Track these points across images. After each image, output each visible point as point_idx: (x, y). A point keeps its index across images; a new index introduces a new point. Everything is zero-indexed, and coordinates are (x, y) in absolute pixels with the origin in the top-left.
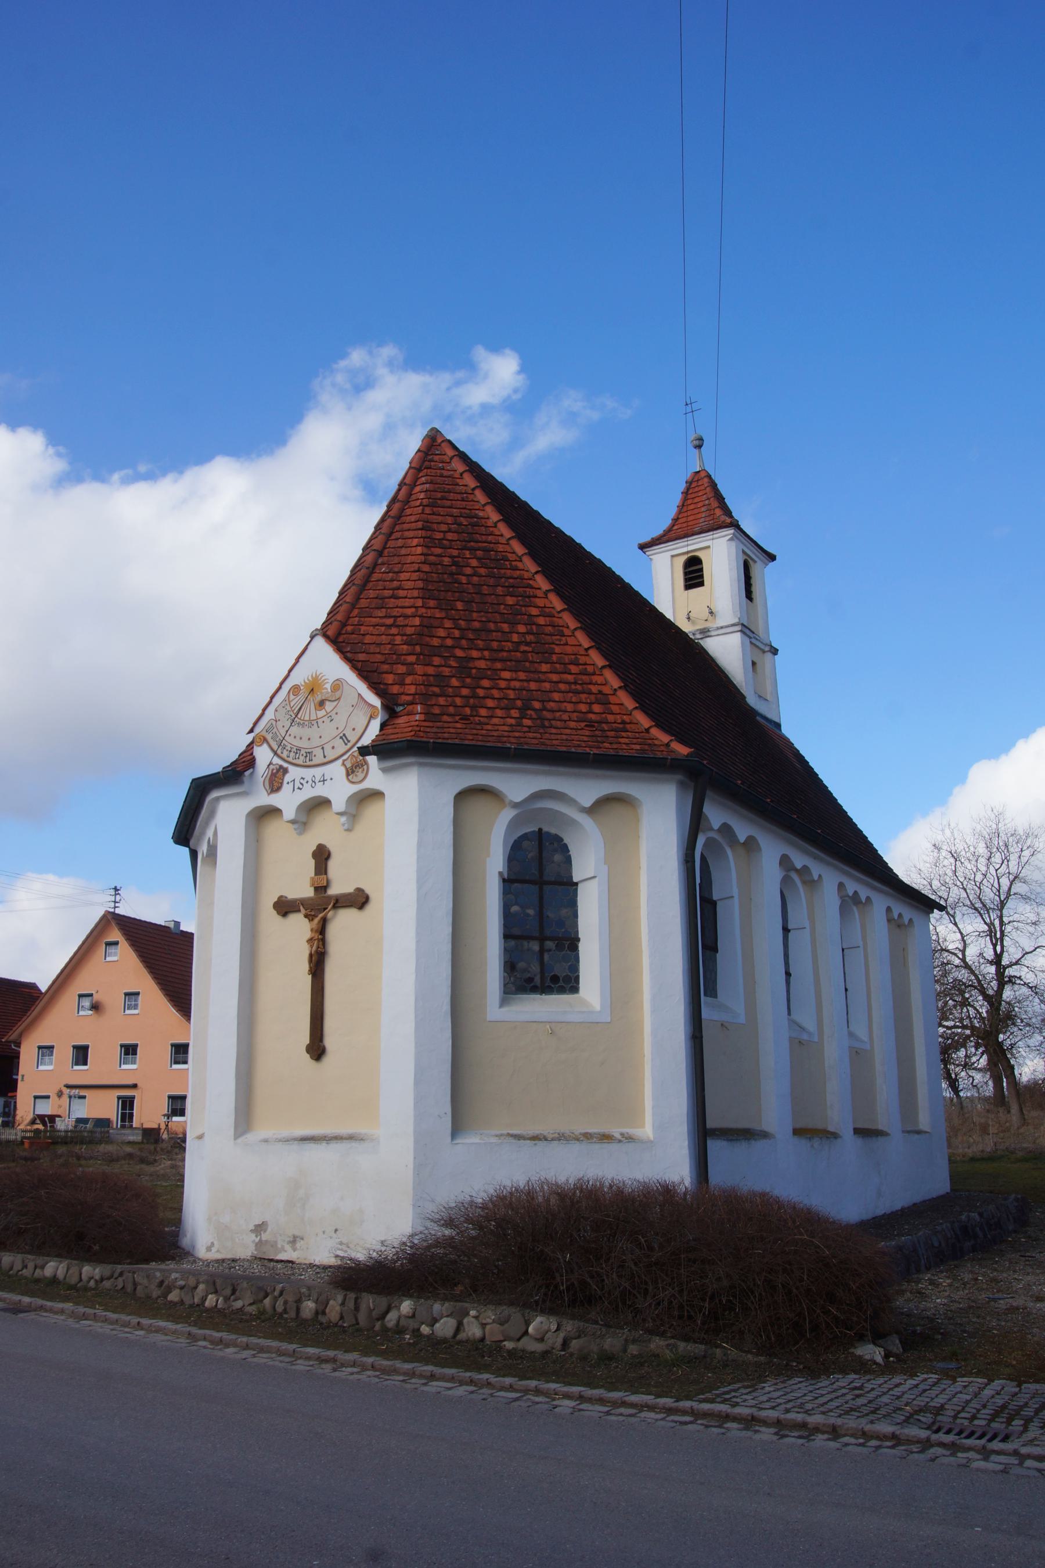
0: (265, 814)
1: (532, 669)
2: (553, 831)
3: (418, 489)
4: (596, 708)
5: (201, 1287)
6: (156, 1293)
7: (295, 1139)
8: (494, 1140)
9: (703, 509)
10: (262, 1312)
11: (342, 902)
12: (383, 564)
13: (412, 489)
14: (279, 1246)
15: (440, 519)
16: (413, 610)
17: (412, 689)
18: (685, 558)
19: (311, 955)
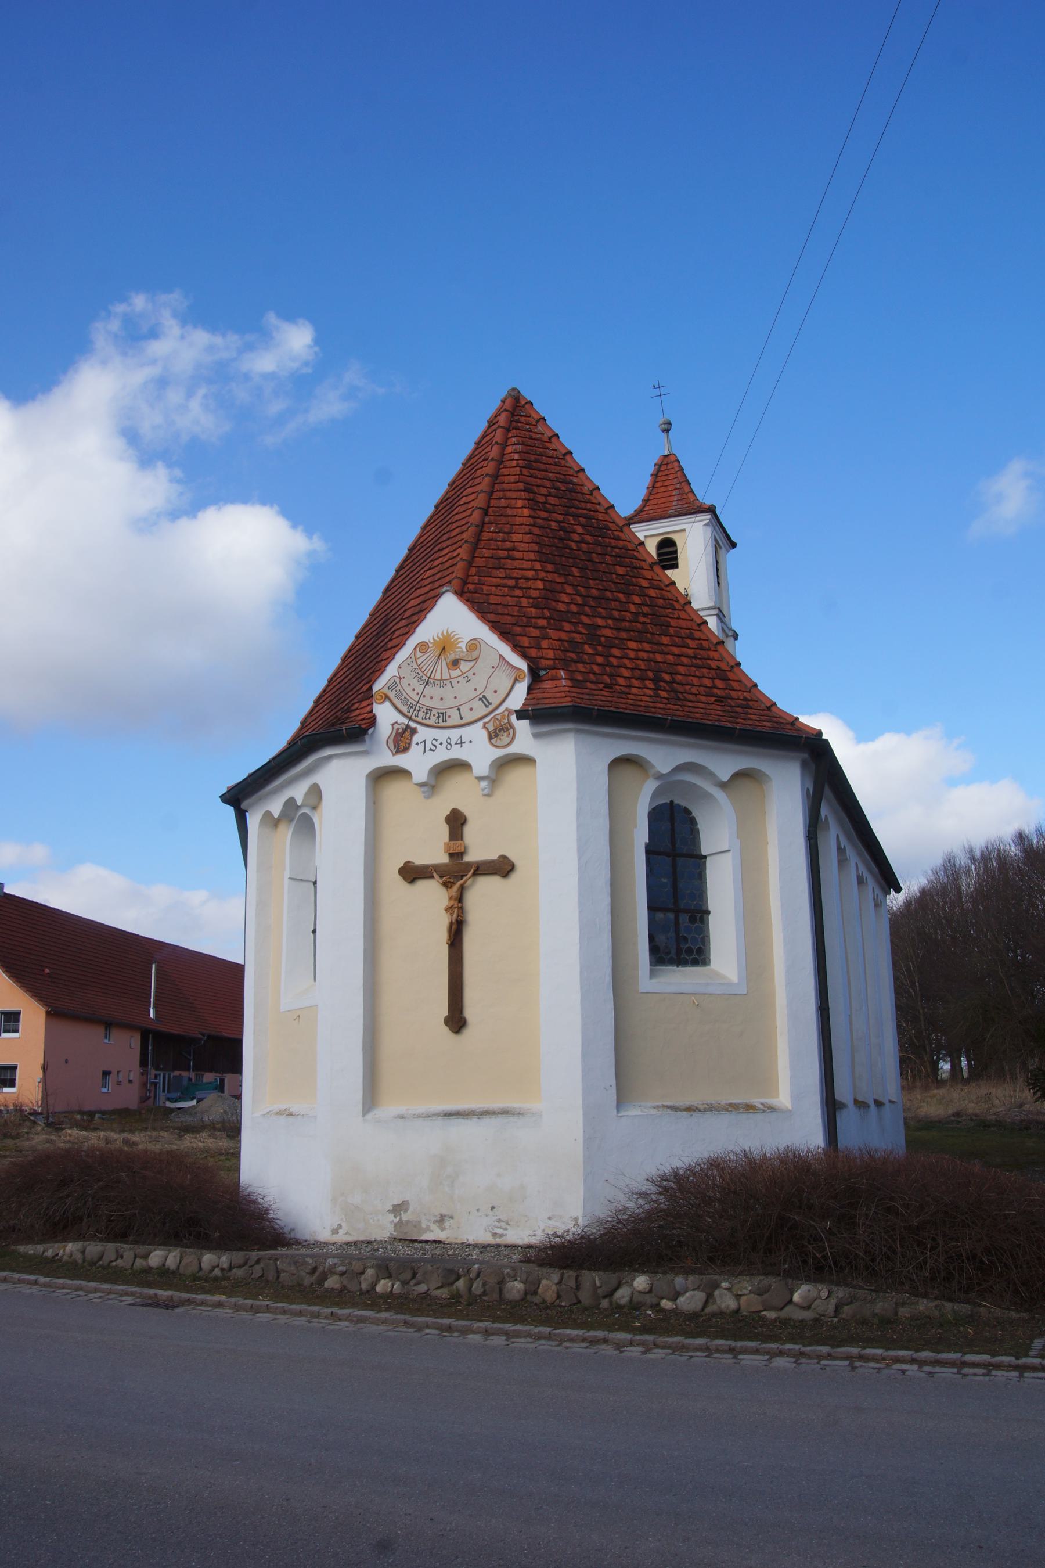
0: (381, 776)
1: (655, 641)
2: (683, 804)
3: (509, 449)
4: (719, 683)
5: (370, 1272)
6: (308, 1280)
7: (438, 1115)
8: (654, 1112)
9: (674, 493)
10: (456, 1296)
11: (482, 869)
12: (490, 523)
13: (503, 449)
14: (424, 1226)
15: (539, 482)
16: (533, 572)
17: (551, 654)
18: (658, 539)
19: (451, 924)
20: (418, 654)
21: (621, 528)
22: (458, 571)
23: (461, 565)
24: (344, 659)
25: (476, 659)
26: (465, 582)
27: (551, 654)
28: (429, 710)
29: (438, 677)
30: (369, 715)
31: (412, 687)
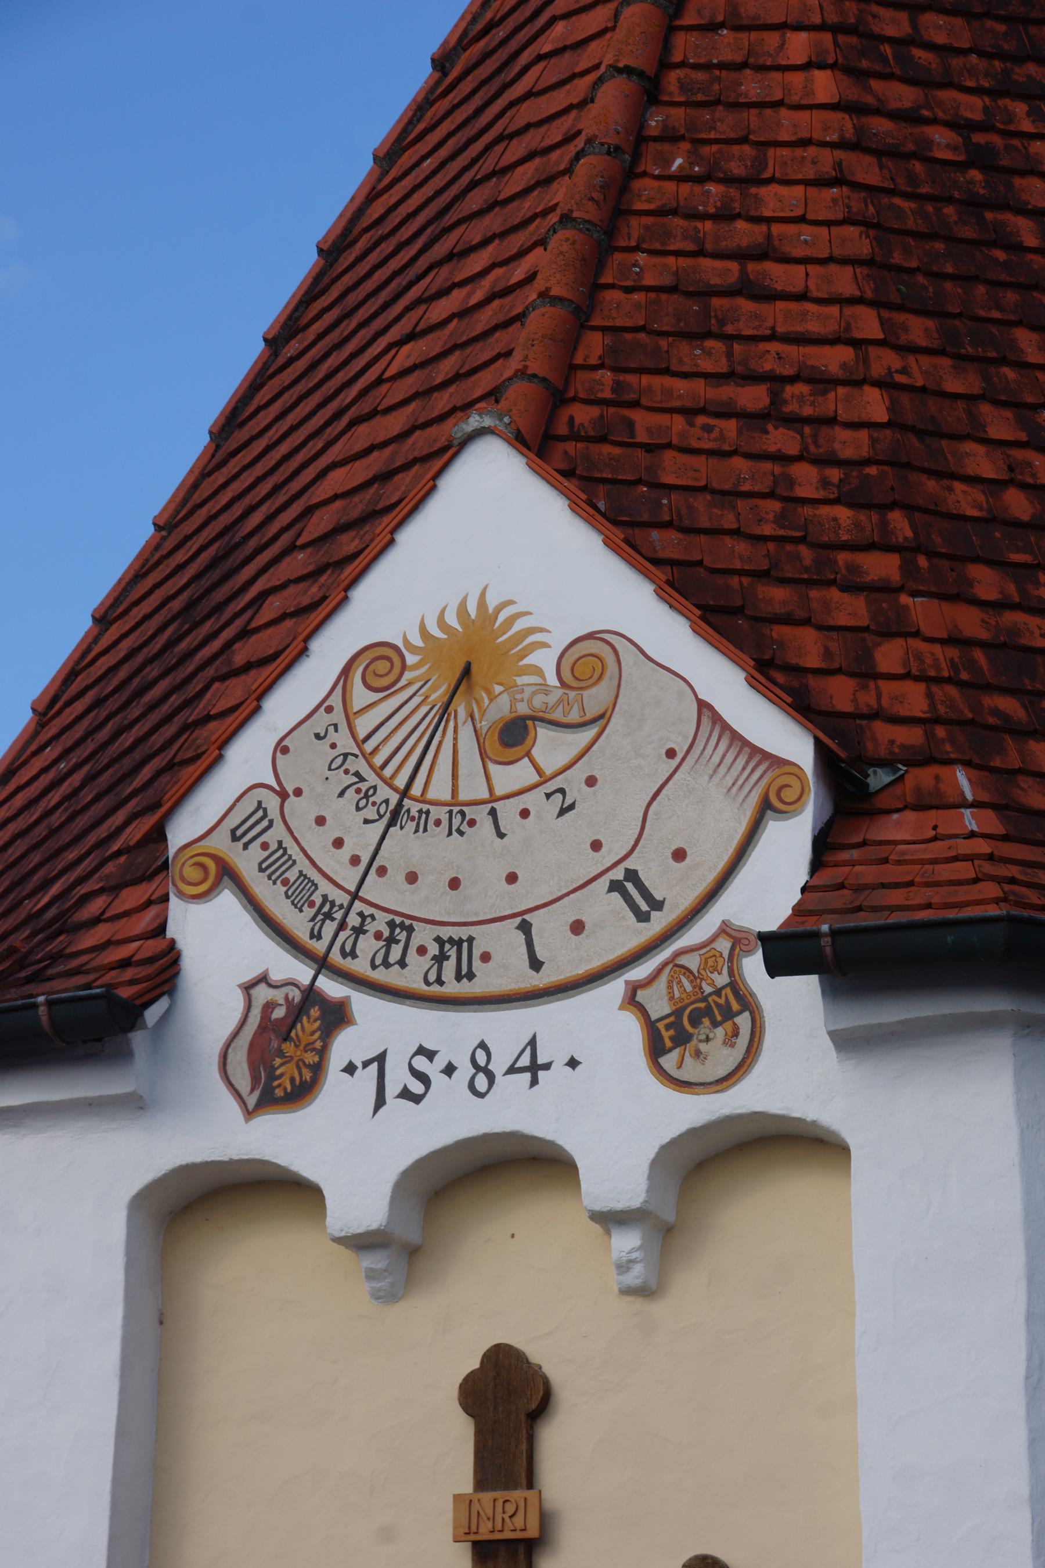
0: (192, 1207)
17: (914, 699)
20: (361, 696)
22: (532, 345)
23: (542, 321)
24: (47, 710)
25: (603, 718)
26: (557, 396)
27: (914, 699)
28: (402, 926)
29: (440, 790)
30: (151, 947)
31: (332, 833)
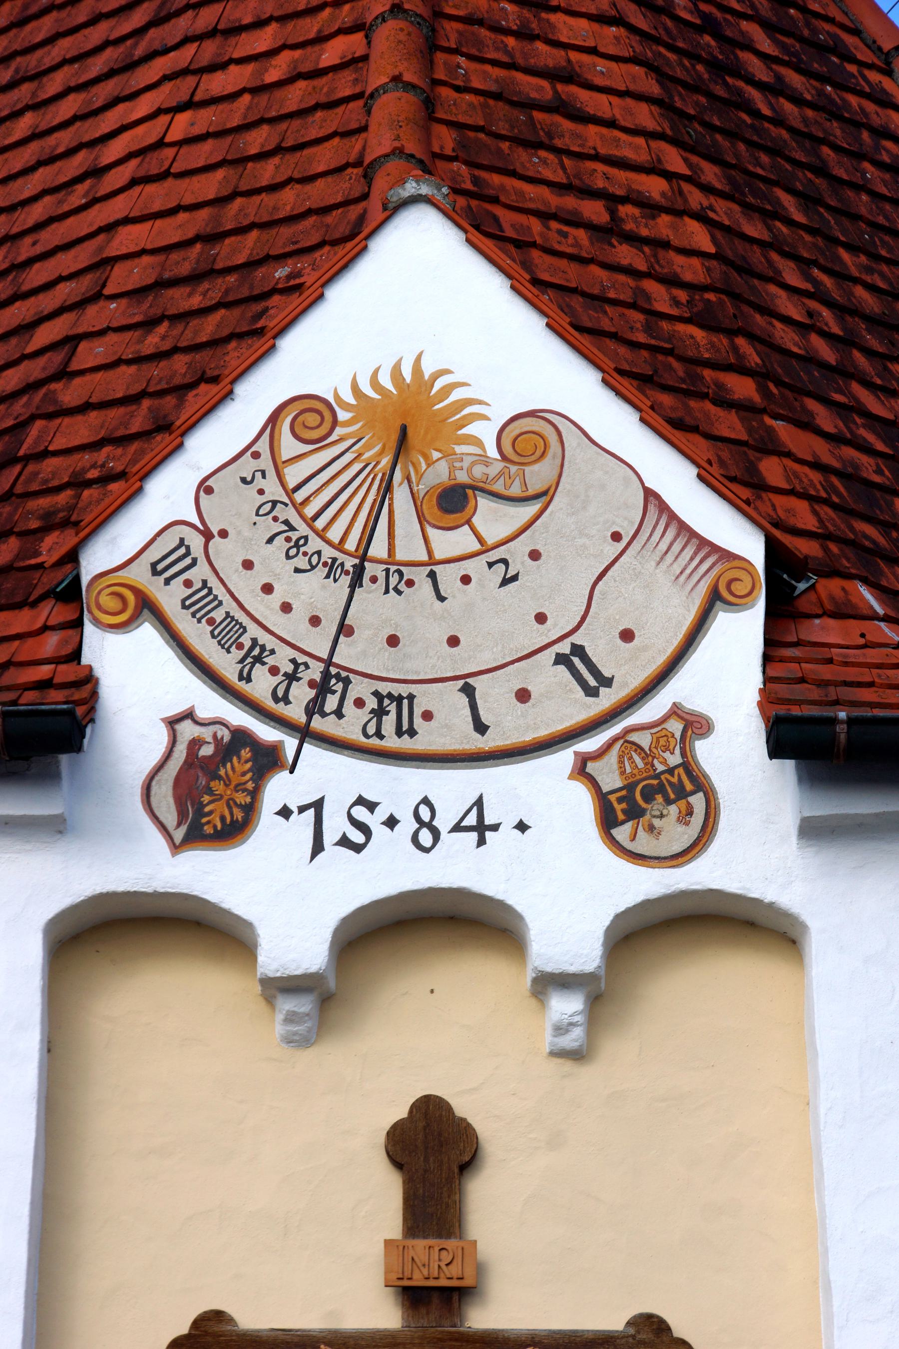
21: (887, 57)
25: (546, 496)
